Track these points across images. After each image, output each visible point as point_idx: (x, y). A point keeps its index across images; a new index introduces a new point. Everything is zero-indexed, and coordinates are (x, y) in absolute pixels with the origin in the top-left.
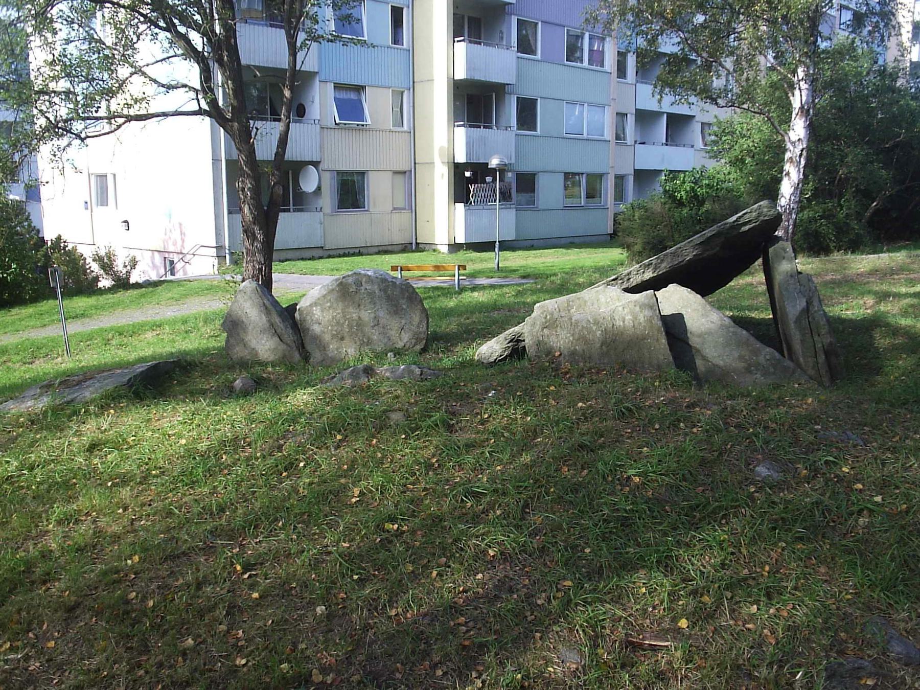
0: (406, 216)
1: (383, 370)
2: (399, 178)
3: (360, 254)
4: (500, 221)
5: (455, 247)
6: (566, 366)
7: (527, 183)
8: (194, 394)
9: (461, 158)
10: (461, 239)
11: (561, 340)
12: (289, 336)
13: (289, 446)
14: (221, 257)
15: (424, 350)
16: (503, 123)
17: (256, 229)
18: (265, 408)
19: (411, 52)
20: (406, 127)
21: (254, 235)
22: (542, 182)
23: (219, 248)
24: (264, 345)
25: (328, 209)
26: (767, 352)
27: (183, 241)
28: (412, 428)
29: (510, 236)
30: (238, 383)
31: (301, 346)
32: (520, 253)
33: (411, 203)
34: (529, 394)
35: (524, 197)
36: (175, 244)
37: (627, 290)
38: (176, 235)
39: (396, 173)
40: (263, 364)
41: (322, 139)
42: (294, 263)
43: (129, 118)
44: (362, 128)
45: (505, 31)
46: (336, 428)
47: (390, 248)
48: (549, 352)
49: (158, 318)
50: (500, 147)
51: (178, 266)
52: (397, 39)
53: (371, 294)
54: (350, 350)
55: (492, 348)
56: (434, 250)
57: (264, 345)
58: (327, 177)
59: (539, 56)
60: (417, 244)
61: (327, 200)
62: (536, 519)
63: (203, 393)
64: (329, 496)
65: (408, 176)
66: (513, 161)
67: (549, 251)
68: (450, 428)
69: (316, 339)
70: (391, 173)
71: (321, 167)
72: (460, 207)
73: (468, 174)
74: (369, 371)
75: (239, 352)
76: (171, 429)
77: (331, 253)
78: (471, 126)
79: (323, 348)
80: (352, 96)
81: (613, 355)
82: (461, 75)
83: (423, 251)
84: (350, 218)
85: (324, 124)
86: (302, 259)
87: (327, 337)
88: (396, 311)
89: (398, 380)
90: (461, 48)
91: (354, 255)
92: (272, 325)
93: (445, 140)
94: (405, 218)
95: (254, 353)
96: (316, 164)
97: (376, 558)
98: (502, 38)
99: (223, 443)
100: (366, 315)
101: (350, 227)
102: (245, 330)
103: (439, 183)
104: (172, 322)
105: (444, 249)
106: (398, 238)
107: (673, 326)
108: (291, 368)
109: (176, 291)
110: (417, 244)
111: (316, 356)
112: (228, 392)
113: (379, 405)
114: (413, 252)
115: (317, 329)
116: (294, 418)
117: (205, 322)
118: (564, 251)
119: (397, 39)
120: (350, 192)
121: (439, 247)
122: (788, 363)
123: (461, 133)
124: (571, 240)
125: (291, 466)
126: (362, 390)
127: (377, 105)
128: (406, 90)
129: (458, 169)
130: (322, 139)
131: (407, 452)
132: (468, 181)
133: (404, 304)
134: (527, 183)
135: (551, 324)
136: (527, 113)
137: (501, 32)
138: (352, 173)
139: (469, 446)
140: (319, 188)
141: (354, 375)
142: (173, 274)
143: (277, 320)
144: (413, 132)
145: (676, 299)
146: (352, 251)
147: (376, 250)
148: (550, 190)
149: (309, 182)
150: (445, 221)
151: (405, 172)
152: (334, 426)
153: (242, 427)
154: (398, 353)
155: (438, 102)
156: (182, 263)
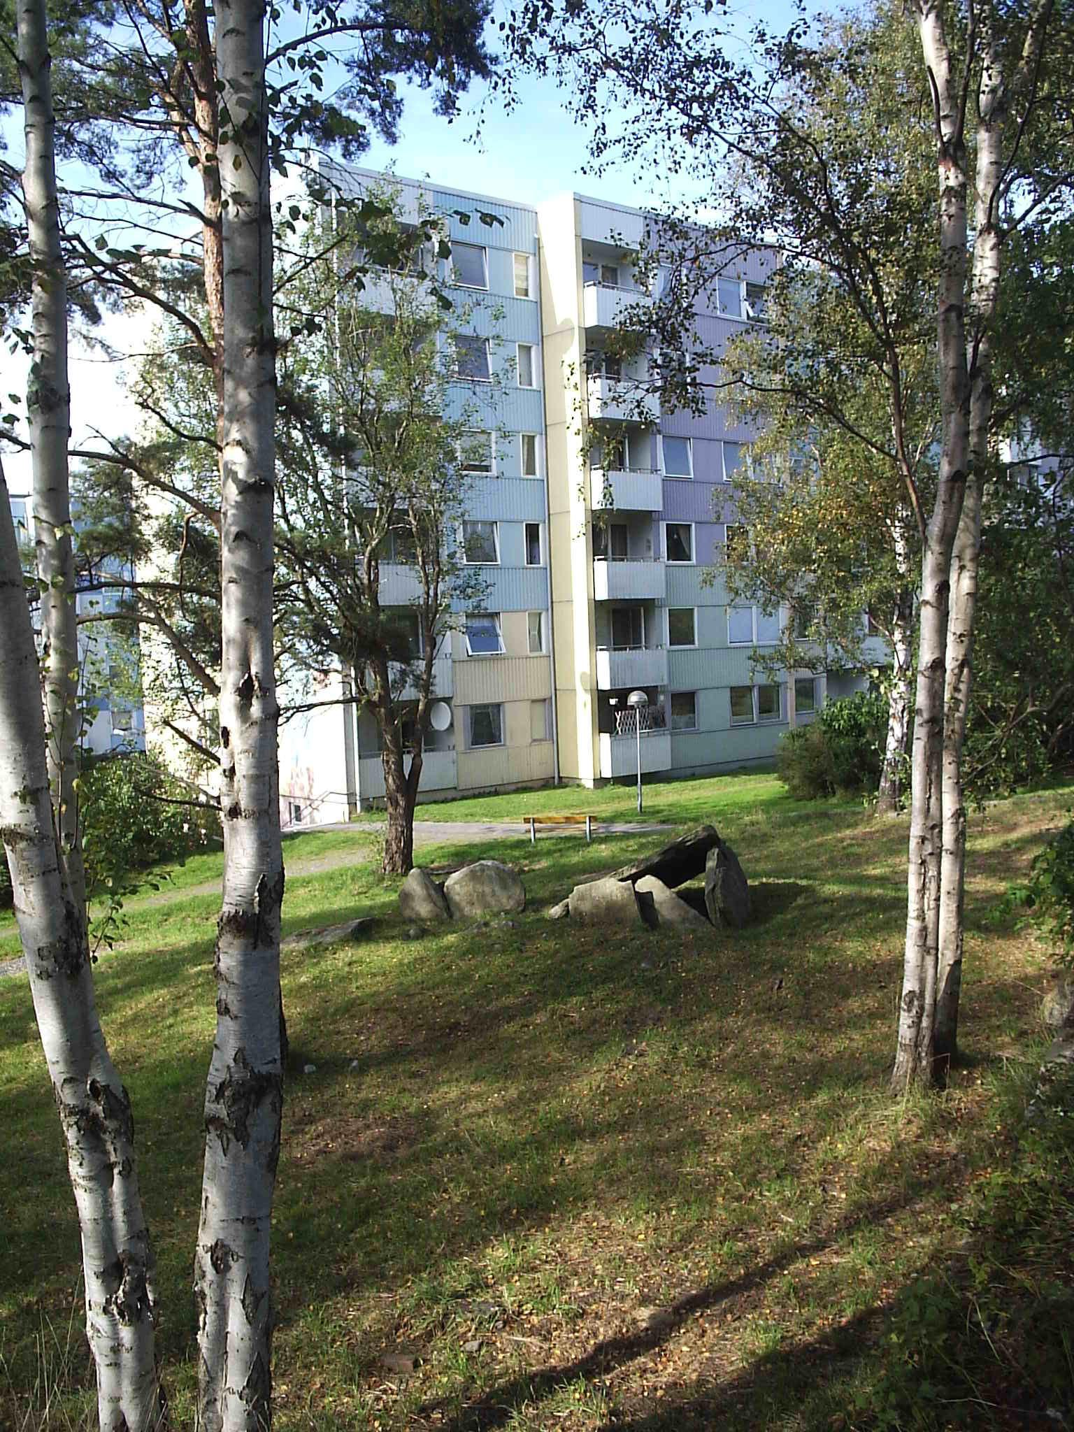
0: (546, 748)
1: (494, 924)
2: (539, 708)
3: (496, 793)
4: (652, 750)
5: (600, 782)
6: (587, 920)
7: (685, 701)
8: (388, 939)
9: (605, 685)
10: (607, 773)
11: (586, 907)
12: (440, 903)
13: (447, 960)
14: (352, 804)
15: (523, 911)
16: (654, 641)
17: (399, 796)
18: (433, 944)
19: (548, 570)
20: (544, 651)
21: (398, 804)
22: (701, 701)
23: (350, 795)
24: (423, 909)
25: (461, 747)
26: (693, 912)
27: (311, 787)
28: (503, 952)
29: (664, 765)
30: (412, 932)
31: (448, 908)
32: (676, 785)
33: (552, 733)
34: (561, 936)
35: (683, 719)
36: (302, 789)
37: (622, 880)
38: (304, 780)
39: (534, 701)
40: (422, 920)
41: (454, 674)
42: (426, 807)
43: (298, 709)
44: (497, 658)
45: (651, 538)
46: (471, 950)
47: (529, 784)
48: (581, 914)
49: (304, 874)
50: (653, 663)
51: (305, 813)
52: (533, 557)
53: (490, 877)
54: (477, 912)
55: (555, 911)
56: (579, 786)
57: (423, 909)
58: (459, 713)
59: (694, 561)
60: (560, 778)
61: (461, 738)
62: (546, 983)
63: (393, 938)
64: (466, 977)
65: (549, 705)
66: (665, 682)
67: (712, 780)
68: (521, 951)
69: (457, 905)
70: (527, 704)
71: (453, 703)
72: (605, 737)
73: (613, 702)
74: (486, 924)
75: (407, 913)
76: (384, 956)
77: (465, 793)
78: (615, 650)
79: (461, 910)
80: (486, 623)
81: (610, 913)
82: (602, 595)
83: (566, 786)
84: (487, 754)
85: (456, 657)
86: (435, 802)
87: (463, 904)
88: (505, 887)
89: (501, 929)
90: (601, 567)
91: (490, 794)
92: (430, 895)
93: (587, 665)
94: (546, 749)
95: (418, 914)
96: (447, 700)
97: (484, 993)
98: (649, 547)
99: (416, 959)
100: (487, 890)
101: (487, 764)
102: (413, 899)
103: (583, 712)
104: (321, 879)
105: (589, 784)
106: (539, 772)
107: (644, 900)
108: (442, 923)
109: (315, 844)
110: (560, 778)
111: (457, 915)
112: (407, 938)
113: (490, 942)
114: (555, 788)
115: (457, 898)
116: (448, 948)
117: (353, 879)
118: (728, 779)
119: (533, 557)
120: (485, 725)
121: (583, 782)
122: (703, 918)
123: (604, 657)
124: (742, 764)
125: (449, 968)
126: (483, 934)
127: (512, 630)
128: (545, 610)
129: (601, 697)
130: (454, 674)
131: (498, 960)
132: (610, 711)
133: (510, 881)
134: (685, 701)
135: (582, 898)
136: (682, 631)
137: (649, 541)
138: (485, 706)
139: (527, 958)
140: (452, 725)
141: (479, 927)
142: (298, 819)
143: (433, 892)
144: (552, 656)
145: (649, 884)
146: (487, 790)
147: (513, 787)
148: (713, 708)
149: (441, 720)
150: (590, 754)
151: (544, 700)
152: (468, 952)
153: (423, 953)
154: (507, 912)
155: (578, 624)
156: (310, 809)
